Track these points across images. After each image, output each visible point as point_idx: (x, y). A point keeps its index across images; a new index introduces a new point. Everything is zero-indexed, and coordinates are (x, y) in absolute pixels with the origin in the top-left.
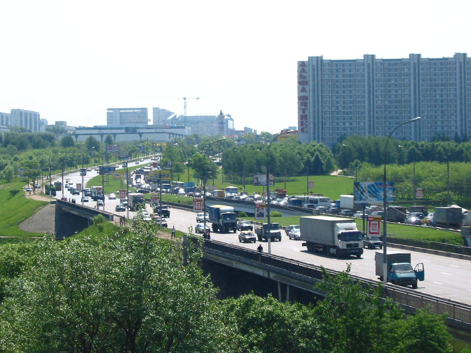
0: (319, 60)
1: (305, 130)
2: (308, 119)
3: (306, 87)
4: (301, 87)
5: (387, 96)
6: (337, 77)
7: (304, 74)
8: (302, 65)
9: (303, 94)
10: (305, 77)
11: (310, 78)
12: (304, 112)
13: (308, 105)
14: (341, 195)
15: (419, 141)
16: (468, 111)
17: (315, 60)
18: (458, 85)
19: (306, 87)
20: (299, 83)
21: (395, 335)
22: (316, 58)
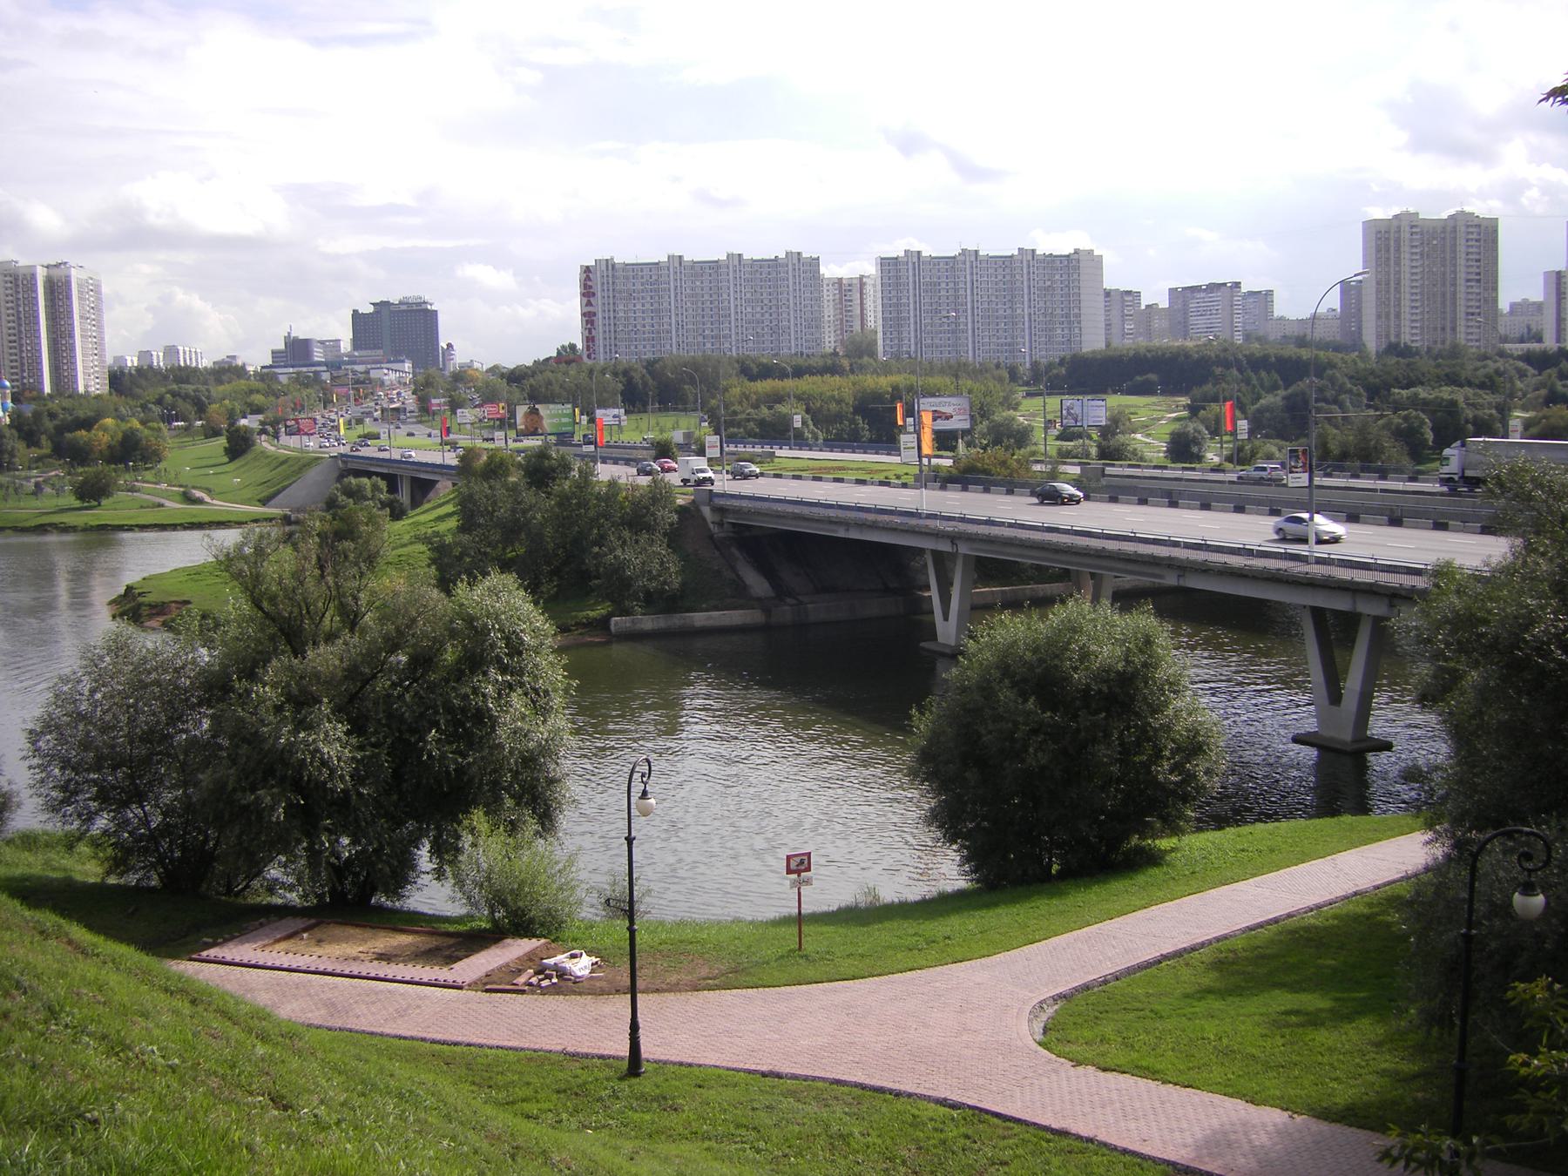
0: (610, 265)
1: (593, 356)
2: (597, 342)
3: (592, 299)
4: (585, 300)
5: (888, 333)
6: (634, 285)
7: (589, 283)
8: (587, 270)
9: (589, 309)
10: (591, 287)
11: (598, 289)
12: (590, 332)
13: (596, 324)
14: (1490, 581)
15: (1279, 531)
16: (487, 440)
17: (604, 263)
18: (912, 306)
19: (592, 299)
20: (583, 295)
21: (917, 1133)
22: (1554, 275)
